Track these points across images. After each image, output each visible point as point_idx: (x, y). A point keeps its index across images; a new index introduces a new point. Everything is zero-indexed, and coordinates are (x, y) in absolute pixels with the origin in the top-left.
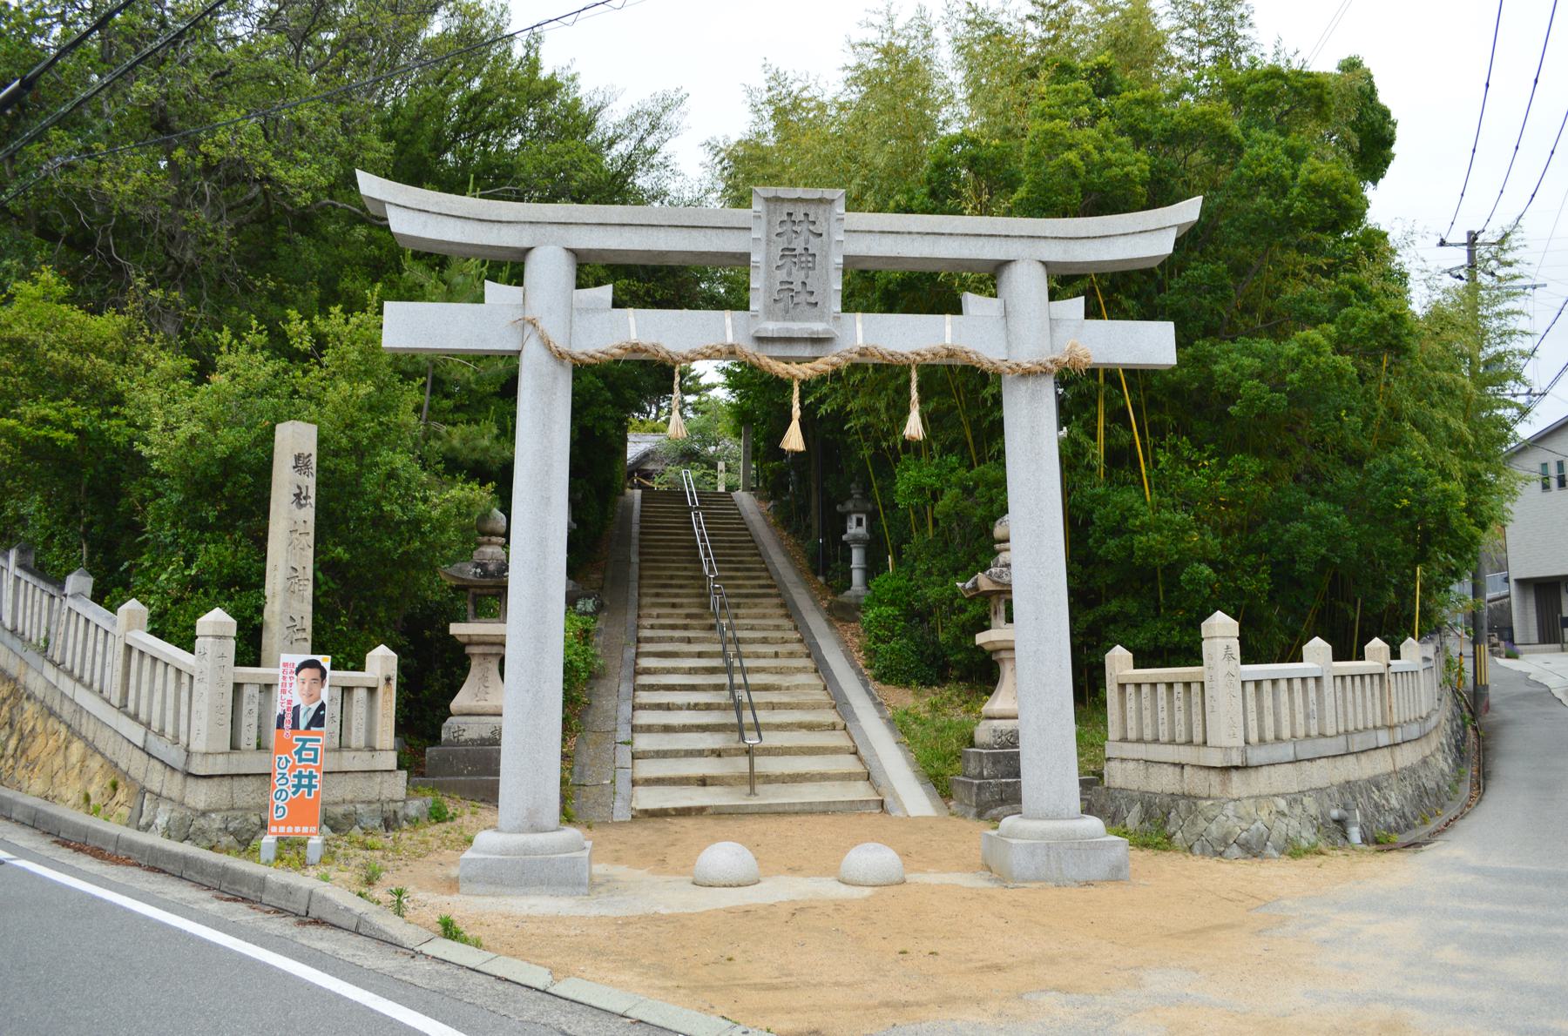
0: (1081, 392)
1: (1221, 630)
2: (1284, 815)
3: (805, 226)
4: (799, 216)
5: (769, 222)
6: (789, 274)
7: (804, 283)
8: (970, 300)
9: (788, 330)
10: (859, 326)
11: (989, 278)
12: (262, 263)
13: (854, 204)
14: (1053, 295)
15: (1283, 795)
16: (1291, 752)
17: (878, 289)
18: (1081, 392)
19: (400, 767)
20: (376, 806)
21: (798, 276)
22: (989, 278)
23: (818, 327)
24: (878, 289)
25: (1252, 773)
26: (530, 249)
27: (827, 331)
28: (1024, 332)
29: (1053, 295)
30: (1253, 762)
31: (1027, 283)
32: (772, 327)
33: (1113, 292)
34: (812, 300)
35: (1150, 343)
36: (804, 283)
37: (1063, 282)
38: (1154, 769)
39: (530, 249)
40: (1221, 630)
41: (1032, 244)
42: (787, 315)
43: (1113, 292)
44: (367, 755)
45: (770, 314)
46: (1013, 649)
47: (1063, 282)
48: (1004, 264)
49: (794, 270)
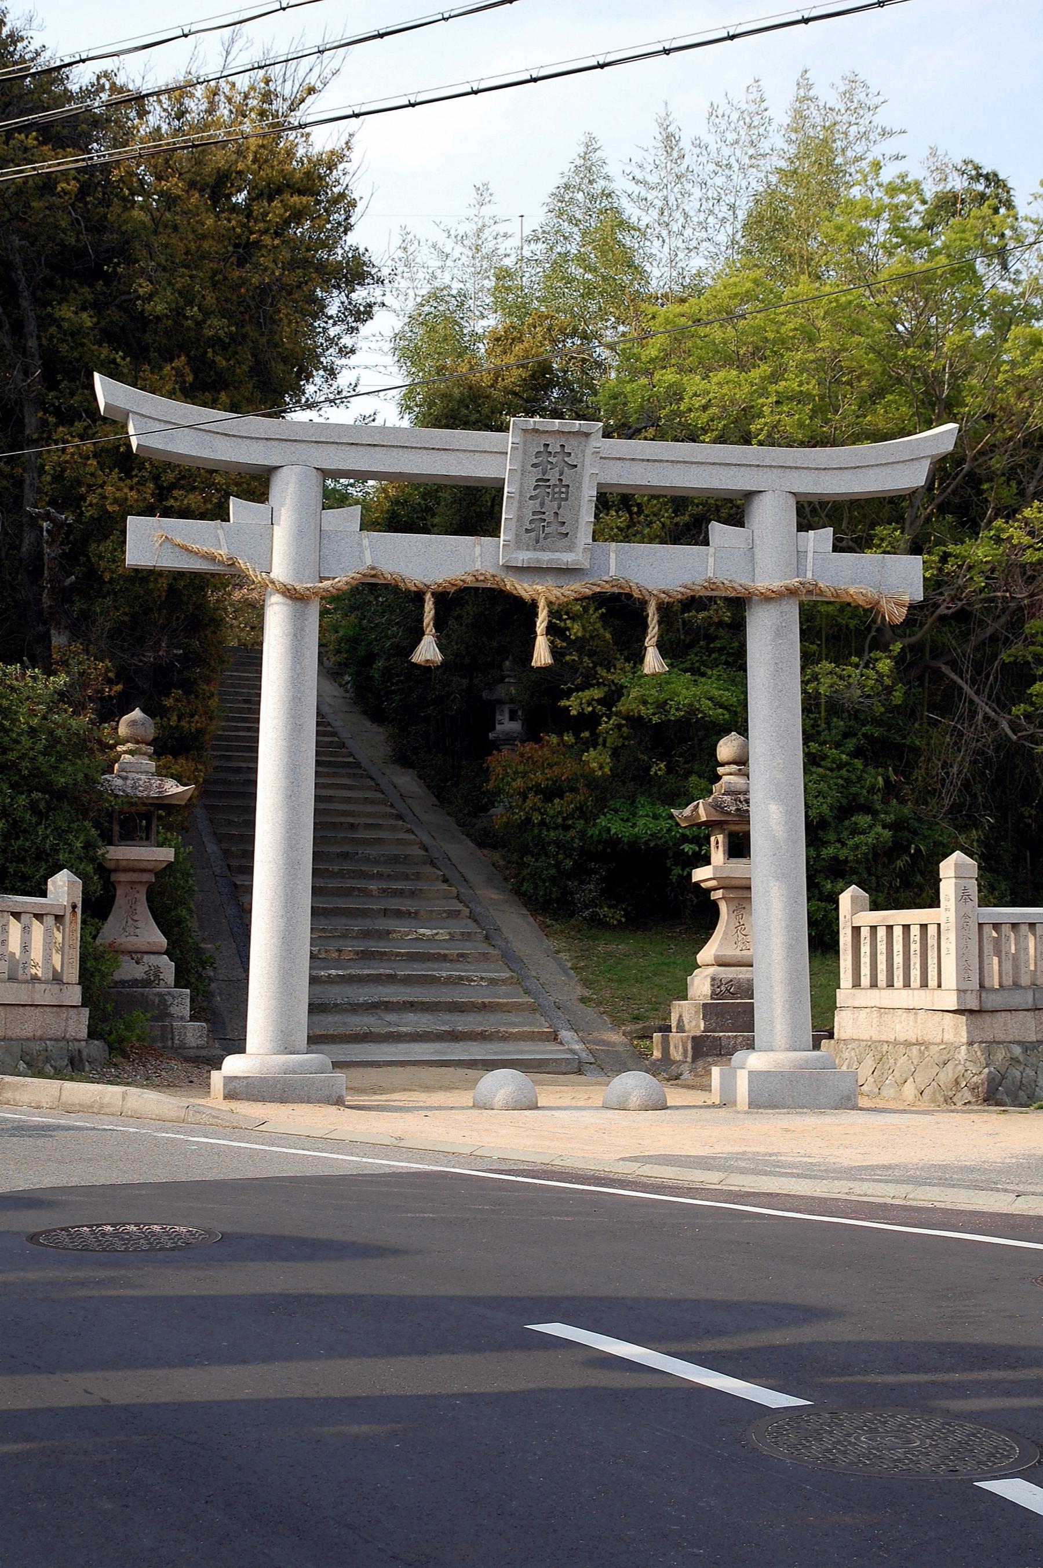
0: (832, 631)
1: (955, 871)
2: (1019, 1062)
3: (560, 457)
4: (555, 448)
5: (525, 453)
6: (542, 504)
7: (556, 513)
8: (717, 530)
9: (538, 560)
10: (613, 555)
11: (733, 509)
12: (90, 432)
13: (607, 435)
14: (802, 527)
15: (1019, 1043)
16: (1030, 999)
17: (626, 513)
18: (832, 631)
19: (84, 1005)
20: (63, 1044)
21: (551, 507)
22: (733, 509)
23: (567, 558)
24: (626, 513)
25: (987, 1017)
26: (277, 468)
27: (577, 562)
28: (767, 557)
29: (802, 527)
30: (989, 1006)
31: (772, 516)
32: (523, 557)
33: (853, 522)
34: (563, 530)
35: (892, 579)
36: (556, 513)
37: (811, 513)
38: (888, 1018)
39: (277, 468)
40: (955, 871)
41: (776, 477)
42: (537, 544)
43: (853, 522)
44: (56, 988)
45: (518, 544)
46: (749, 888)
47: (811, 513)
48: (749, 495)
49: (547, 500)
